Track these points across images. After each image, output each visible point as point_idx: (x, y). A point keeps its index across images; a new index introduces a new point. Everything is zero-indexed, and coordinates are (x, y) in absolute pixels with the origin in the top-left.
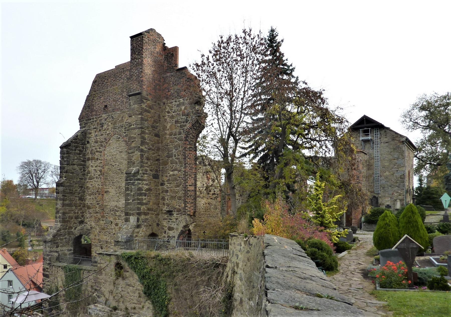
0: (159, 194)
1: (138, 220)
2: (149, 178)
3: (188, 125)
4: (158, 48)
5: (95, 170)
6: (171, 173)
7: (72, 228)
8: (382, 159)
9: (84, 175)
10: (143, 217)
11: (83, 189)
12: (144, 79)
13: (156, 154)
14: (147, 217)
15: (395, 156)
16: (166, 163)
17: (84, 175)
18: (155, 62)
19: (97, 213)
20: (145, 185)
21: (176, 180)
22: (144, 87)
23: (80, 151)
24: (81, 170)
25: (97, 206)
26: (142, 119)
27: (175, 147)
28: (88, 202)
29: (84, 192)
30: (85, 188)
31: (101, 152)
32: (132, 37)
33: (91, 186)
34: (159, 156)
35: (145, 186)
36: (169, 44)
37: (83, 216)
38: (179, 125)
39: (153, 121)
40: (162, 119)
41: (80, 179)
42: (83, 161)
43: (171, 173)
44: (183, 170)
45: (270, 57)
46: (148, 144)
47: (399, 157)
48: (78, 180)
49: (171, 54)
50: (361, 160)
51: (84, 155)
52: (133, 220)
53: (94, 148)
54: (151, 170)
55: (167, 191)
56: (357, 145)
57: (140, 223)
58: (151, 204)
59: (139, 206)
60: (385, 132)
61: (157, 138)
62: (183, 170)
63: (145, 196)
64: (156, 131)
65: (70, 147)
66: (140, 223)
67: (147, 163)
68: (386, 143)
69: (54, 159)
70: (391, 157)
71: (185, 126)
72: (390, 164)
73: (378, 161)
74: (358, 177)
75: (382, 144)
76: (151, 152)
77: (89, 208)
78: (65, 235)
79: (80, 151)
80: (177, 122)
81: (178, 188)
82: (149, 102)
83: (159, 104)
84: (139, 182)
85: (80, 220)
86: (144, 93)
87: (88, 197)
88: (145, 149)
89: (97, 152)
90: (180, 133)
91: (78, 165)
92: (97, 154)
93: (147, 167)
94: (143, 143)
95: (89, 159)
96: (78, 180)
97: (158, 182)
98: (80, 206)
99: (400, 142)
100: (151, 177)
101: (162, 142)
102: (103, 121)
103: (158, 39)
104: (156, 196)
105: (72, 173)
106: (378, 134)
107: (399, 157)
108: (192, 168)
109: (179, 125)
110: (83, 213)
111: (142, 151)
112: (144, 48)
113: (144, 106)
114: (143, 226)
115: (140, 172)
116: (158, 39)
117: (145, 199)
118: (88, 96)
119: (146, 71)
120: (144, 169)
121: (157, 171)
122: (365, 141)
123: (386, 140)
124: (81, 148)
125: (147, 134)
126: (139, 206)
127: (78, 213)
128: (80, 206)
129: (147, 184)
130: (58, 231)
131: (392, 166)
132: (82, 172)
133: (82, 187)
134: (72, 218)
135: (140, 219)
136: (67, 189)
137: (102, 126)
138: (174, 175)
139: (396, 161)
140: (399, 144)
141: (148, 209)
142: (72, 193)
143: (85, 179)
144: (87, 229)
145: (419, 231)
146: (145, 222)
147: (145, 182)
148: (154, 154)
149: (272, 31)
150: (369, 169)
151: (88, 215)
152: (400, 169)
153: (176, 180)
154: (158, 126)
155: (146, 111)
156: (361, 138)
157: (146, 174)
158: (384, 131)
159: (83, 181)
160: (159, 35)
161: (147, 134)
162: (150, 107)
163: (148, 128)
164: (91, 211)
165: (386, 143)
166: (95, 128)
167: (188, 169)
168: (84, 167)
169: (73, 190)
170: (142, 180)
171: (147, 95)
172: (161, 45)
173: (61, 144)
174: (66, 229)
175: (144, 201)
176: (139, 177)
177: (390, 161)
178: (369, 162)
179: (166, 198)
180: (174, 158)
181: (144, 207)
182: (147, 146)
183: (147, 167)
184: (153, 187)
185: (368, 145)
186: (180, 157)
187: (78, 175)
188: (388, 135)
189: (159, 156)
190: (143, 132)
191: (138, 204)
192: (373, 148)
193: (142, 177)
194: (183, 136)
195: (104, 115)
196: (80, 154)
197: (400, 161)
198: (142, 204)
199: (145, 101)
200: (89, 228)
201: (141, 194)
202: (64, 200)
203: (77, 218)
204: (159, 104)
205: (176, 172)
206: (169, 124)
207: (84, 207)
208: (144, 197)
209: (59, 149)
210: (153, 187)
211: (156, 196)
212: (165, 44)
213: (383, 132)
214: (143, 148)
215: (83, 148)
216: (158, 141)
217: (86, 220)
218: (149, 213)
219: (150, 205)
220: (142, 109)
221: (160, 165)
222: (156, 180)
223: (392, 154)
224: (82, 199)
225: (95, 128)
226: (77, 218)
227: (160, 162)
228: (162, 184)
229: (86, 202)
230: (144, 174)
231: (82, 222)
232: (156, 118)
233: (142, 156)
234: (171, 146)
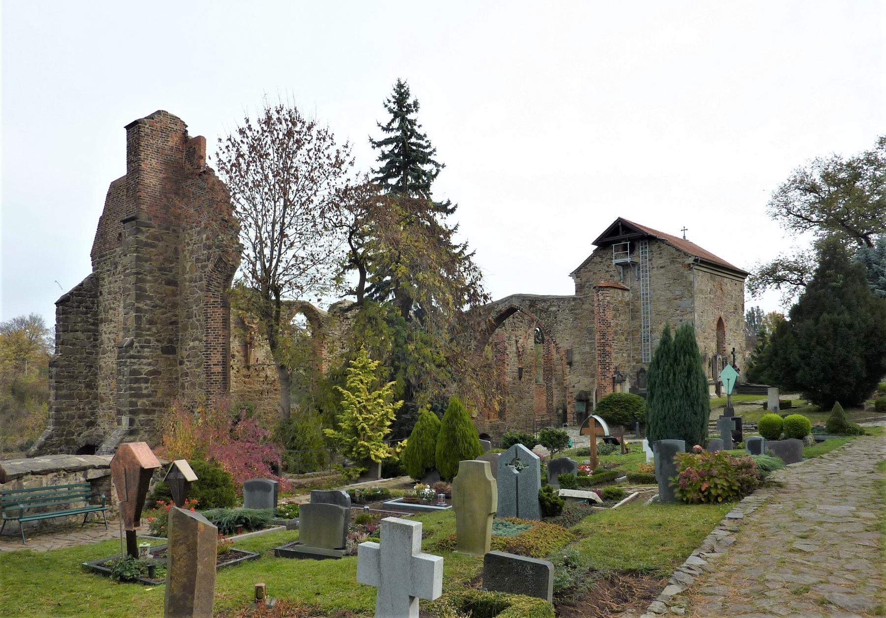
0: (177, 379)
1: (132, 422)
2: (155, 354)
3: (211, 266)
4: (173, 141)
5: (109, 338)
6: (191, 344)
7: (73, 434)
8: (654, 298)
9: (96, 346)
10: (142, 417)
11: (93, 369)
12: (143, 194)
13: (169, 314)
14: (150, 417)
15: (677, 293)
16: (185, 329)
17: (96, 346)
18: (166, 163)
19: (111, 409)
20: (145, 364)
21: (197, 355)
22: (144, 207)
23: (87, 308)
24: (89, 338)
25: (111, 397)
26: (138, 259)
27: (196, 301)
28: (101, 391)
29: (96, 374)
30: (97, 368)
31: (115, 309)
32: (127, 127)
33: (104, 365)
34: (176, 316)
35: (145, 367)
36: (192, 133)
37: (93, 414)
38: (200, 265)
39: (161, 261)
40: (181, 256)
41: (88, 353)
42: (93, 324)
43: (191, 344)
44: (205, 339)
45: (399, 133)
46: (151, 298)
47: (683, 294)
48: (85, 355)
49: (193, 147)
50: (608, 302)
51: (96, 314)
52: (125, 420)
53: (107, 303)
54: (157, 341)
55: (187, 375)
56: (612, 273)
57: (135, 427)
58: (159, 395)
59: (134, 399)
60: (659, 247)
61: (170, 287)
62: (205, 339)
63: (147, 383)
64: (170, 276)
65: (69, 303)
66: (135, 427)
67: (149, 329)
68: (662, 267)
69: (50, 320)
70: (670, 295)
71: (206, 266)
72: (668, 308)
73: (647, 304)
74: (604, 335)
75: (655, 271)
76: (158, 311)
77: (102, 401)
78: (60, 445)
79: (87, 308)
80: (198, 260)
81: (198, 370)
82: (152, 230)
83: (174, 231)
84: (133, 360)
85: (88, 420)
86: (143, 217)
87: (101, 383)
88: (146, 307)
89: (111, 309)
90: (201, 280)
91: (83, 332)
92: (111, 312)
93: (149, 335)
94: (139, 298)
95: (102, 321)
96: (85, 355)
97: (175, 360)
98: (88, 397)
99: (685, 266)
100: (159, 352)
101: (181, 294)
102: (117, 259)
103: (173, 126)
104: (170, 382)
105: (74, 344)
106: (646, 253)
107: (683, 294)
108: (217, 337)
109: (200, 265)
110: (94, 408)
111: (138, 310)
112: (142, 144)
113: (142, 237)
114: (142, 432)
115: (136, 344)
116: (173, 126)
117: (147, 388)
118: (101, 218)
119: (147, 181)
120: (143, 339)
121: (170, 341)
122: (625, 266)
123: (660, 262)
124: (89, 304)
125: (149, 281)
126: (134, 399)
127: (83, 409)
128: (88, 397)
129: (149, 364)
130: (47, 439)
131: (672, 311)
132: (90, 342)
133: (91, 366)
134: (73, 418)
135: (137, 420)
136: (63, 372)
137: (116, 268)
138: (194, 348)
139: (678, 302)
140: (682, 270)
141: (153, 404)
142: (72, 377)
143: (97, 354)
144: (98, 436)
145: (457, 445)
146: (147, 425)
147: (145, 361)
148: (164, 313)
149: (400, 86)
150: (633, 318)
151: (101, 413)
152: (685, 317)
153: (197, 355)
154: (173, 267)
155: (147, 245)
156: (614, 261)
157: (148, 347)
158: (656, 246)
159: (94, 356)
160: (175, 120)
161: (149, 281)
162: (156, 238)
163: (150, 272)
164: (104, 404)
165: (662, 267)
166: (108, 270)
167: (211, 338)
168: (95, 335)
169: (74, 372)
170: (140, 357)
171: (150, 220)
172: (180, 133)
173: (57, 298)
174: (62, 435)
175: (145, 392)
176: (132, 353)
177: (669, 301)
178: (634, 306)
179: (186, 384)
180: (194, 319)
181: (145, 400)
182: (148, 302)
183: (149, 335)
184: (161, 366)
185: (630, 274)
186: (201, 317)
187: (83, 347)
188: (665, 253)
189: (176, 316)
190: (139, 280)
191: (131, 396)
192: (639, 279)
193: (139, 352)
194: (204, 282)
195: (118, 249)
196: (86, 313)
197: (685, 303)
198: (140, 396)
199: (144, 229)
200: (102, 434)
201: (137, 381)
202: (57, 388)
203: (81, 417)
204: (174, 231)
205: (197, 342)
206: (189, 264)
207: (96, 398)
208: (143, 385)
209: (55, 307)
210: (161, 366)
211: (170, 382)
212: (186, 131)
213: (655, 247)
214: (140, 305)
215: (93, 303)
216: (173, 291)
217: (99, 421)
218: (155, 411)
219: (158, 398)
220: (138, 242)
221: (177, 331)
222: (171, 356)
223: (671, 288)
224: (92, 385)
225: (108, 270)
226: (81, 417)
227: (179, 325)
228: (181, 363)
229: (100, 391)
230: (142, 347)
231: (91, 424)
232: (170, 253)
233: (138, 319)
234: (191, 300)
